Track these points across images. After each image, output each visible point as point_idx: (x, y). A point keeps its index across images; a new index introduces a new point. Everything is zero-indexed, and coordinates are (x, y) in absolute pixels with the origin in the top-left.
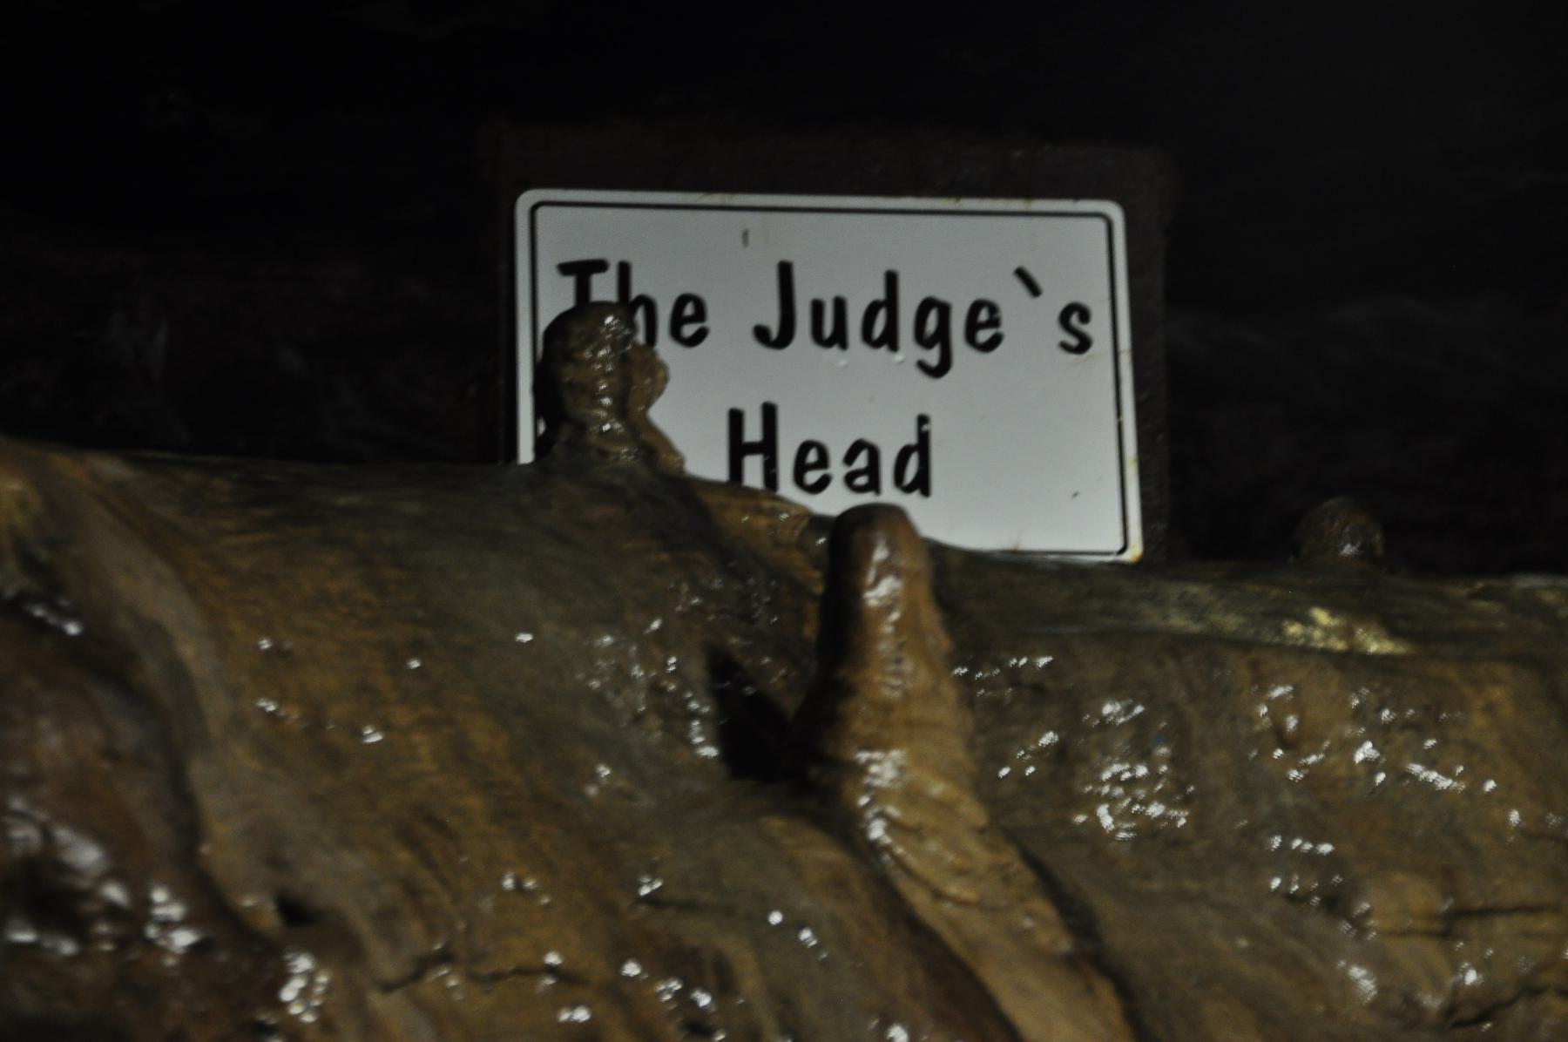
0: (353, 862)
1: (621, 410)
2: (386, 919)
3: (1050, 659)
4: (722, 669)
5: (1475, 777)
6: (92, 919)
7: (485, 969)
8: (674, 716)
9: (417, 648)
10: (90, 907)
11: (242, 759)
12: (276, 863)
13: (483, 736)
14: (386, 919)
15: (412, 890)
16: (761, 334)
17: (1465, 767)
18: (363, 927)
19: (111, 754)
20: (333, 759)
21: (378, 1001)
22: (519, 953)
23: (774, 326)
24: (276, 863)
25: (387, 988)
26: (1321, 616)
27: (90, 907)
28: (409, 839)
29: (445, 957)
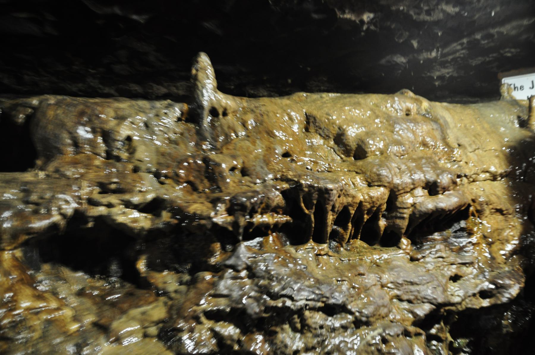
0: (467, 139)
1: (508, 93)
2: (470, 145)
3: (204, 59)
4: (519, 117)
5: (18, 343)
6: (430, 147)
7: (484, 150)
8: (513, 123)
9: (479, 117)
10: (429, 145)
11: (455, 130)
12: (457, 140)
13: (486, 126)
14: (470, 145)
15: (474, 142)
16: (530, 88)
17: (218, 241)
18: (467, 146)
19: (433, 129)
20: (467, 129)
21: (469, 154)
22: (489, 148)
23: (531, 86)
24: (457, 140)
25: (471, 152)
26: (509, 55)
27: (429, 145)
28: (474, 136)
29: (478, 149)
